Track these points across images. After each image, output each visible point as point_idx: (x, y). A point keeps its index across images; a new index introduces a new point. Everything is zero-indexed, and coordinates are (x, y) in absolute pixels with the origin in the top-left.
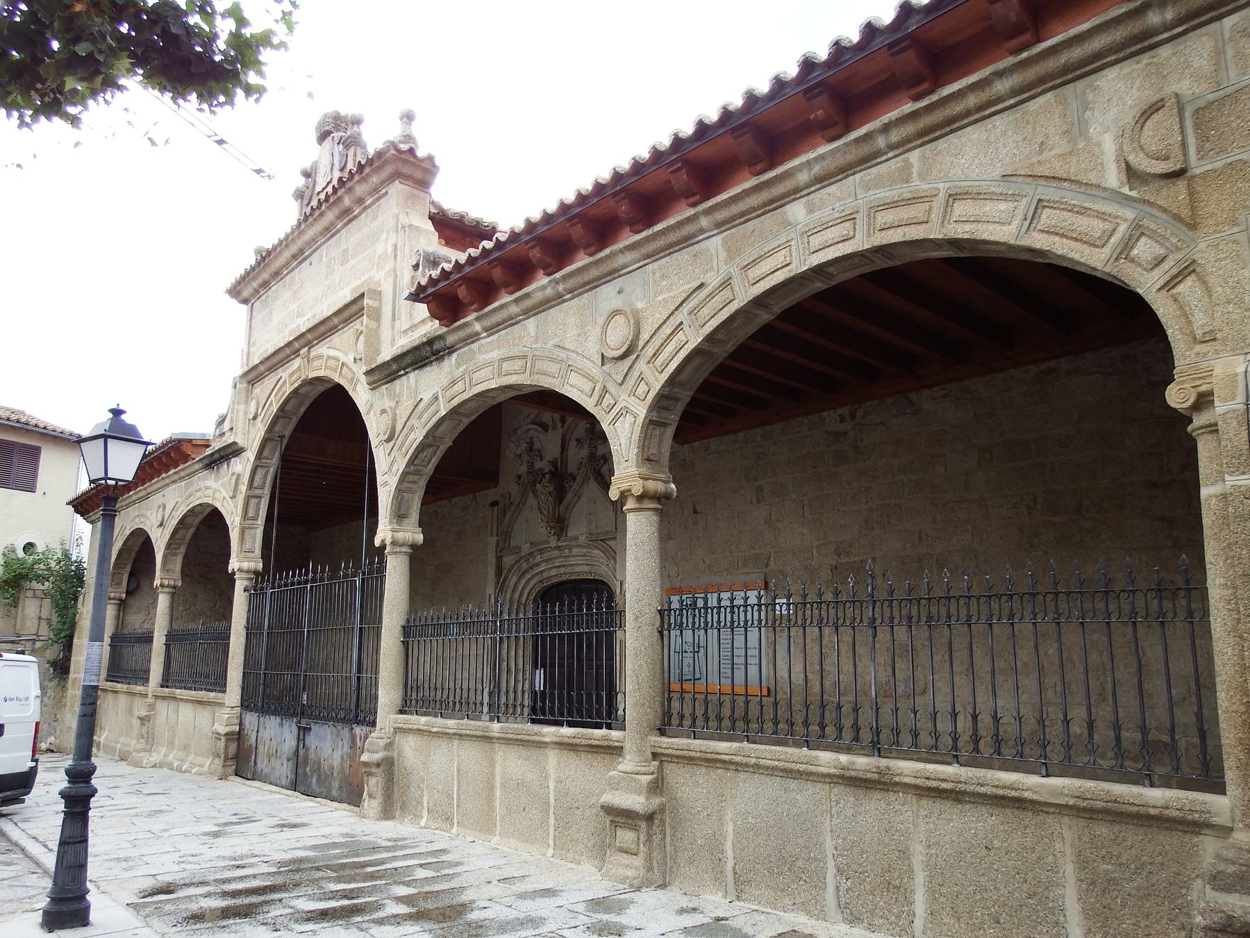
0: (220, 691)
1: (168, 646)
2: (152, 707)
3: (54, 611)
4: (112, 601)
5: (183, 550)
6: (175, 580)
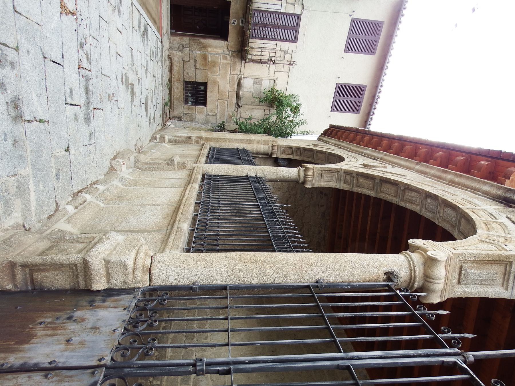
0: (189, 242)
1: (247, 178)
2: (182, 166)
3: (259, 121)
4: (271, 148)
5: (343, 186)
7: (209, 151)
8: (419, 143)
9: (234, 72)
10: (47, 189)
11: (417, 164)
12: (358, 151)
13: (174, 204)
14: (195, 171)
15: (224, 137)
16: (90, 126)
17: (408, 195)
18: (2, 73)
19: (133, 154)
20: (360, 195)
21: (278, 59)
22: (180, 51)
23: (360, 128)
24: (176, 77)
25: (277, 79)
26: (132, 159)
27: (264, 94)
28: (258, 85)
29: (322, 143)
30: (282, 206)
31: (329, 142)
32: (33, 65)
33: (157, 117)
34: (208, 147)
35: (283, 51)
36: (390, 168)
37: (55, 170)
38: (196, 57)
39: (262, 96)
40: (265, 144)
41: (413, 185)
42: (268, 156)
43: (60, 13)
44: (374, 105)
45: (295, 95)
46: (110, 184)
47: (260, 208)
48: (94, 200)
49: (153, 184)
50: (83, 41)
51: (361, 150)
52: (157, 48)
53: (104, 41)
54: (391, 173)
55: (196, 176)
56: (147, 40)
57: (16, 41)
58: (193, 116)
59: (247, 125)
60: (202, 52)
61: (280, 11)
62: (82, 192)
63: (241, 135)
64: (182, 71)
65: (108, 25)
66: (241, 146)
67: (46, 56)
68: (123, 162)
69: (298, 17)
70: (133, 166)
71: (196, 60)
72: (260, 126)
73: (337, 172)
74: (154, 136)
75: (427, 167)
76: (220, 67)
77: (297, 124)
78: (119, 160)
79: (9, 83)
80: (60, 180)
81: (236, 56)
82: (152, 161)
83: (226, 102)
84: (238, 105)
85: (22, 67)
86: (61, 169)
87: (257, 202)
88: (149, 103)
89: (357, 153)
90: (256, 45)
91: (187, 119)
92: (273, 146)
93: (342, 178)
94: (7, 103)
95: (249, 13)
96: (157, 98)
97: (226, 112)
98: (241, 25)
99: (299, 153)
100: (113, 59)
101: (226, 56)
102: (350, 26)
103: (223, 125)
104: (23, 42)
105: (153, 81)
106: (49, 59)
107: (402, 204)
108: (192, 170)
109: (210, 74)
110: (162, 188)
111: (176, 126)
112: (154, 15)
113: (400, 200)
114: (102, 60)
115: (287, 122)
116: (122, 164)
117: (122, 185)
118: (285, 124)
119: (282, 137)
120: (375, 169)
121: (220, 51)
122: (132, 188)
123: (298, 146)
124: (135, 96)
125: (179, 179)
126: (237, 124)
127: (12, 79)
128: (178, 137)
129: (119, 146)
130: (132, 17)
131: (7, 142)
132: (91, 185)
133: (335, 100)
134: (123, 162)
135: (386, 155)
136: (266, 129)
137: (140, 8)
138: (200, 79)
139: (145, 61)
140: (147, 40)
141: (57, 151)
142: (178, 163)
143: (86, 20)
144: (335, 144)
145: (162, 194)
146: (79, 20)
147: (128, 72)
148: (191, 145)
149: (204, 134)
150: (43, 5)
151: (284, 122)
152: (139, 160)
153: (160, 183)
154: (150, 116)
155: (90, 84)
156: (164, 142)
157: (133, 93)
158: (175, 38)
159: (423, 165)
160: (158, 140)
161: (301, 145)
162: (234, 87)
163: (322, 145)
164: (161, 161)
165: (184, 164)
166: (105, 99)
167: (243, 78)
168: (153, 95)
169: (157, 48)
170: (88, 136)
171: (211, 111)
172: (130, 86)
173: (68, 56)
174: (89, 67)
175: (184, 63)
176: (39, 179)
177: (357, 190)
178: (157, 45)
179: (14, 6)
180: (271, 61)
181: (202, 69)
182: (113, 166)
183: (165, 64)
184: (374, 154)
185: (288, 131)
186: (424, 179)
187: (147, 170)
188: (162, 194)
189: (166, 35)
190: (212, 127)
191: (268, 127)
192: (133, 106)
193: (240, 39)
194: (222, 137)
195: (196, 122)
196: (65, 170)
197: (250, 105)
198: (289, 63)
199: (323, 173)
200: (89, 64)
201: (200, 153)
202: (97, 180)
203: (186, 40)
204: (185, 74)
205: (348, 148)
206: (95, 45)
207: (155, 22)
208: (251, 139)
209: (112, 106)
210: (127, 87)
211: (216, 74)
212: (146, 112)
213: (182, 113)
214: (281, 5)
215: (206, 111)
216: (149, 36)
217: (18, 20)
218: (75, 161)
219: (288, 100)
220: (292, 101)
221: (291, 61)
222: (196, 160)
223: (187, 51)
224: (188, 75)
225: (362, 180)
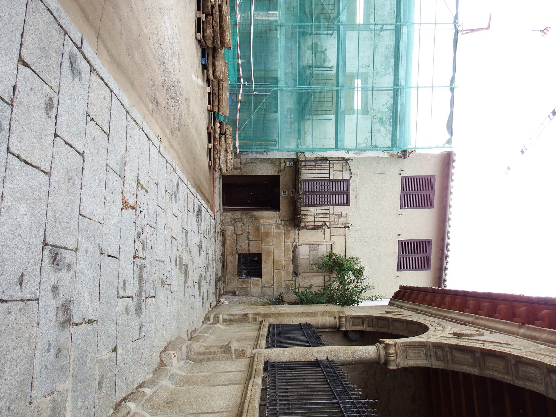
1: (317, 363)
2: (241, 354)
3: (320, 289)
5: (436, 364)
6: (396, 360)
7: (269, 331)
8: (513, 301)
9: (287, 241)
10: (86, 404)
11: (520, 327)
12: (441, 316)
13: (235, 409)
14: (256, 359)
15: (284, 312)
16: (140, 318)
17: (523, 371)
18: (58, 277)
19: (185, 343)
20: (456, 374)
21: (332, 223)
22: (233, 225)
23: (436, 288)
24: (229, 251)
25: (334, 243)
26: (184, 349)
27: (322, 260)
28: (314, 251)
29: (395, 309)
30: (368, 402)
31: (403, 306)
32: (90, 263)
33: (210, 295)
34: (267, 325)
35: (337, 215)
36: (488, 336)
37: (98, 377)
38: (248, 230)
39: (320, 262)
40: (330, 316)
41: (526, 357)
42: (336, 330)
43: (120, 209)
44: (445, 258)
45: (356, 258)
46: (159, 385)
47: (340, 407)
48: (139, 411)
49: (207, 382)
50: (141, 231)
51: (445, 314)
52: (210, 225)
53: (161, 227)
54: (491, 342)
55: (258, 367)
56: (201, 220)
57: (77, 243)
58: (248, 289)
59: (308, 295)
60: (254, 224)
61: (329, 178)
62: (126, 399)
63: (302, 307)
64: (234, 244)
65: (164, 212)
66: (304, 320)
67: (103, 252)
68: (174, 354)
69: (347, 182)
70: (185, 357)
71: (248, 233)
72: (322, 294)
73: (425, 347)
74: (207, 316)
75: (535, 330)
76: (273, 237)
77: (363, 289)
78: (169, 352)
79: (62, 286)
80: (102, 389)
81: (289, 225)
82: (206, 349)
83: (283, 272)
84: (295, 274)
85: (78, 267)
86: (105, 375)
87: (335, 399)
88: (203, 281)
89: (440, 318)
90: (309, 212)
91: (241, 293)
92: (340, 317)
93: (432, 354)
94: (58, 308)
95: (299, 184)
96: (210, 275)
97: (283, 282)
98: (291, 195)
99: (371, 324)
100: (168, 243)
101: (279, 225)
102: (401, 184)
103: (281, 297)
104: (83, 242)
105: (206, 257)
106: (106, 255)
107: (518, 383)
108: (253, 358)
109: (263, 244)
110: (218, 385)
111: (230, 303)
112: (207, 196)
113: (514, 378)
114: (157, 246)
115: (351, 288)
116: (173, 356)
117: (172, 384)
118: (350, 290)
119: (348, 305)
120: (469, 338)
121: (273, 221)
122: (184, 388)
123: (369, 315)
124: (189, 277)
125: (238, 372)
126: (296, 295)
127: (67, 281)
128: (234, 315)
129: (170, 336)
130: (187, 200)
131: (50, 353)
132: (137, 388)
133: (400, 258)
134: (174, 354)
135: (477, 318)
136: (329, 297)
137: (194, 192)
138: (253, 251)
139: (199, 239)
140: (201, 220)
141: (103, 353)
142: (236, 350)
143: (145, 211)
144: (412, 308)
145: (220, 396)
146: (138, 212)
147: (182, 254)
148: (248, 323)
149: (261, 310)
150: (106, 204)
151: (348, 288)
152: (192, 350)
153: (216, 378)
154: (203, 295)
155: (144, 272)
156: (219, 322)
157: (186, 274)
158: (228, 213)
159: (528, 328)
160: (212, 320)
161: (372, 313)
162: (290, 256)
163: (397, 312)
164: (216, 350)
165: (243, 350)
166: (158, 285)
167: (298, 245)
168: (206, 272)
169: (210, 225)
170: (138, 329)
171: (267, 282)
172: (183, 267)
173: (124, 248)
174: (145, 255)
175: (236, 236)
176: (78, 393)
177: (454, 368)
178: (210, 222)
179: (80, 210)
180: (324, 226)
181: (255, 241)
182: (163, 360)
183: (218, 239)
184: (462, 318)
185: (354, 297)
186: (536, 346)
187: (201, 361)
188: (220, 396)
189: (219, 211)
190: (270, 300)
191: (331, 295)
192: (186, 287)
193: (292, 208)
194: (281, 312)
195: (252, 295)
196: (110, 375)
197: (308, 272)
198: (344, 226)
199: (407, 349)
200: (144, 252)
201: (259, 334)
202: (144, 381)
203: (238, 214)
204: (238, 247)
205: (428, 312)
206: (151, 233)
207: (208, 201)
208: (315, 311)
209: (165, 291)
210: (181, 269)
211: (270, 244)
212: (199, 291)
213: (236, 287)
214: (329, 173)
215: (262, 283)
216: (203, 215)
217: (82, 222)
218: (122, 362)
219: (349, 263)
220: (353, 264)
221: (346, 224)
222: (256, 343)
223: (239, 224)
224: (242, 247)
225: (457, 354)
